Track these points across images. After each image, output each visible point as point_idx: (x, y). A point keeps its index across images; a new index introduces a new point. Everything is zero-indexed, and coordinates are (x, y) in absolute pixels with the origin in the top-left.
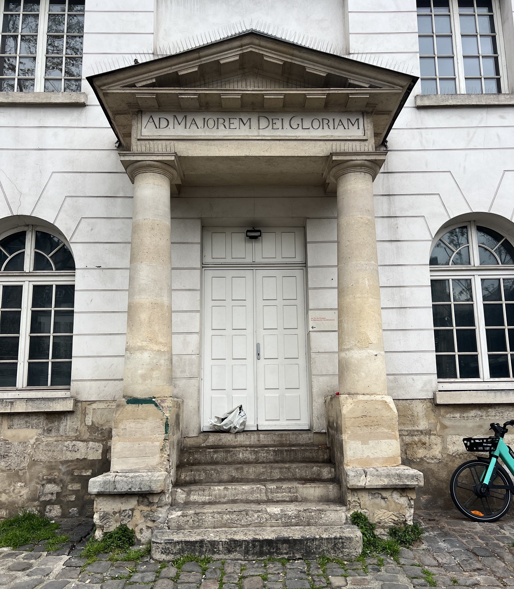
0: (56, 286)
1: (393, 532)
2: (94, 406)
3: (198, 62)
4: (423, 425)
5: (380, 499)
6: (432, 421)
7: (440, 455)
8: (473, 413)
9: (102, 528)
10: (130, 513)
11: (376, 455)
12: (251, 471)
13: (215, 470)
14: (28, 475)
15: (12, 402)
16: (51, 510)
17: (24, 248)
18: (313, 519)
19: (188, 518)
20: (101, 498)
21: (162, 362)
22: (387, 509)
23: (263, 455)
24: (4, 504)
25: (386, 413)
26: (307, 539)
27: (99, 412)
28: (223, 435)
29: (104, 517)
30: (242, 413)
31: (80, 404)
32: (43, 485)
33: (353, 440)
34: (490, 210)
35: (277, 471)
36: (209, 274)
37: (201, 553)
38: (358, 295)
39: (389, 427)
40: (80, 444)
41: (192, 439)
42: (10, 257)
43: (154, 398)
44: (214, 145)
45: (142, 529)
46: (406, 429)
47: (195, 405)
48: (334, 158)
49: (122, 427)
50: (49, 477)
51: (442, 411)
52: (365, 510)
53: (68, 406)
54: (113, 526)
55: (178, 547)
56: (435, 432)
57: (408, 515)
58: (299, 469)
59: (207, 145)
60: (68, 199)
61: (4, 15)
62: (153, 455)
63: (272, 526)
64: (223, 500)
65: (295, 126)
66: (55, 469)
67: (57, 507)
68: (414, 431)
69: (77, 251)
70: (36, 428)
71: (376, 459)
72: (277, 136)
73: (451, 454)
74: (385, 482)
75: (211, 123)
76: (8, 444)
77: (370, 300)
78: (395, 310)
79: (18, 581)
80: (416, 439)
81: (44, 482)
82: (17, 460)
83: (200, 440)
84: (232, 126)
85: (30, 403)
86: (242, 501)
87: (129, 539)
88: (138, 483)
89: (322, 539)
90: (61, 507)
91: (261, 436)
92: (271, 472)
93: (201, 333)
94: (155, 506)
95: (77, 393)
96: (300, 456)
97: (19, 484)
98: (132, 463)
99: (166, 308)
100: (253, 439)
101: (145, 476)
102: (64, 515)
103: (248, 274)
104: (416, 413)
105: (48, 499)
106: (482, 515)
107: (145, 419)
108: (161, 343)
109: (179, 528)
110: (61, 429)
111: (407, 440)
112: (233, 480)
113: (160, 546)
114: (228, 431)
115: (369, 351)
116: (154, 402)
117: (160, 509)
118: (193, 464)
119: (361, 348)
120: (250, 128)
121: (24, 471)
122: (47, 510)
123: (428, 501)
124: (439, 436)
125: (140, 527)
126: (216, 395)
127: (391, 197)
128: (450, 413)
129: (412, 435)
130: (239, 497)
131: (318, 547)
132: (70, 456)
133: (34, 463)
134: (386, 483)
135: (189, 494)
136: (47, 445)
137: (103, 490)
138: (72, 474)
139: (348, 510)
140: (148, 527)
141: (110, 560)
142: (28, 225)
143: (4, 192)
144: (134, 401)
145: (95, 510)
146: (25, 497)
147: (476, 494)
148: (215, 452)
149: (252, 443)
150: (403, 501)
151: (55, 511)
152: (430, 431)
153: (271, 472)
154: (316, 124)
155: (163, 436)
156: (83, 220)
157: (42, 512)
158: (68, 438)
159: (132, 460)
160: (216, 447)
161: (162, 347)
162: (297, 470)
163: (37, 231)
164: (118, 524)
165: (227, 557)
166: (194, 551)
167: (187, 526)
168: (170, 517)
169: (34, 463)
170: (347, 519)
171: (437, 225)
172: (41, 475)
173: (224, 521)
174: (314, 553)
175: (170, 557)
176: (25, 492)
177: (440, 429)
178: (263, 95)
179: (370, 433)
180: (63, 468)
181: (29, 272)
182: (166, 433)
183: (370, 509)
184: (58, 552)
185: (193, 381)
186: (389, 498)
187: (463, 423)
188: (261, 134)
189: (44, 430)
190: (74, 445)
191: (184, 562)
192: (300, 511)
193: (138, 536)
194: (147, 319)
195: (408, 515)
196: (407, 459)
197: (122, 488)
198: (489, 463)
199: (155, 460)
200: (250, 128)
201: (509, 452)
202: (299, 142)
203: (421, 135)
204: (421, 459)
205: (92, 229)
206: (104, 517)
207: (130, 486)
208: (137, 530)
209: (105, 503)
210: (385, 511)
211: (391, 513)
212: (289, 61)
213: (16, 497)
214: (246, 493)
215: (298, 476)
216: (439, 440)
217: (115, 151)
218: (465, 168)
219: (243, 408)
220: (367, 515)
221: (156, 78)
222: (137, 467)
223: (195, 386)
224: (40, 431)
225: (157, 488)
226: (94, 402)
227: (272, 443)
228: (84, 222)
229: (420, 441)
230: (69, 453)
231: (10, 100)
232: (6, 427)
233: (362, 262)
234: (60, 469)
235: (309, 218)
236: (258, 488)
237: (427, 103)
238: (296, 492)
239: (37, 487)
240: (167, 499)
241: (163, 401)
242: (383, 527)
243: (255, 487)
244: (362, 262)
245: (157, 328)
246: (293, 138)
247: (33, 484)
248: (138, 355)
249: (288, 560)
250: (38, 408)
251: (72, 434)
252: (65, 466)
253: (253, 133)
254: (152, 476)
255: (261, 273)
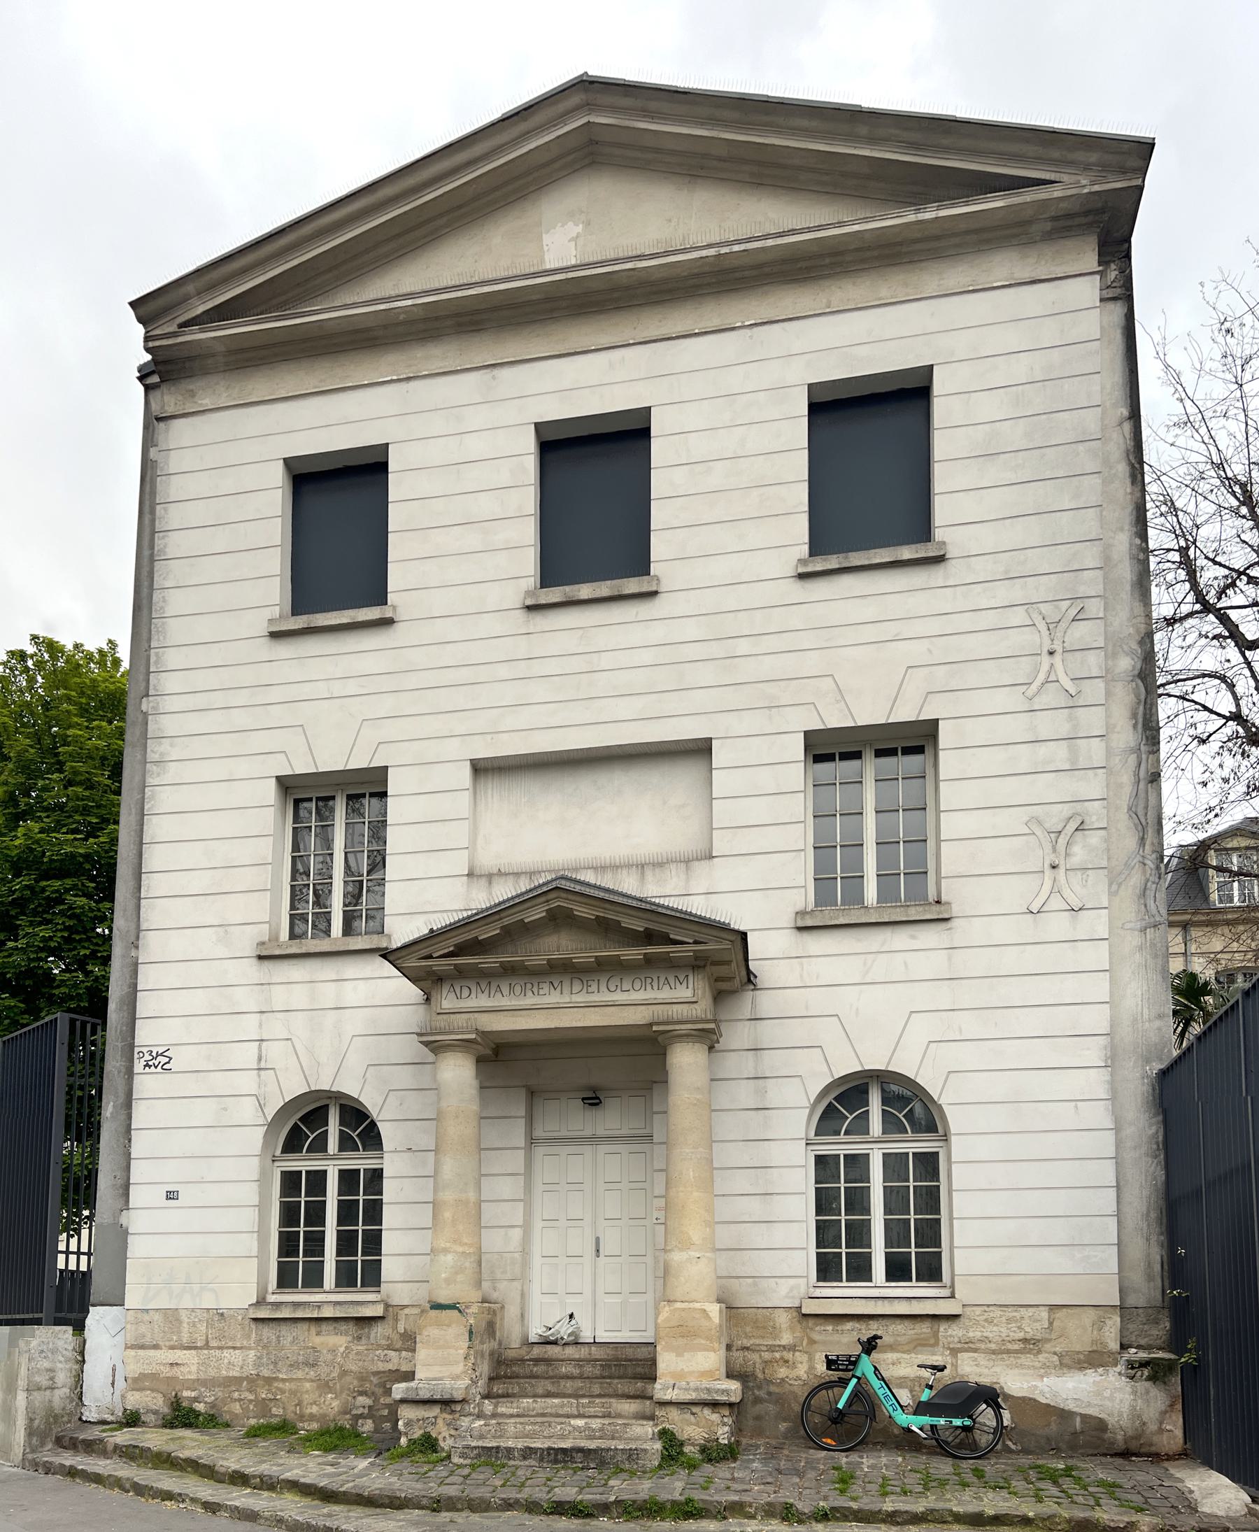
0: (364, 1170)
1: (703, 1450)
2: (407, 1311)
3: (499, 924)
4: (786, 1339)
5: (689, 1414)
6: (798, 1334)
7: (805, 1375)
8: (849, 1325)
9: (406, 1434)
10: (434, 1420)
11: (691, 1369)
12: (569, 1386)
13: (529, 1383)
14: (338, 1386)
15: (319, 1305)
16: (363, 1425)
17: (327, 1125)
18: (618, 1433)
19: (490, 1428)
20: (405, 1405)
21: (467, 1264)
22: (697, 1425)
23: (588, 1369)
24: (316, 1416)
25: (705, 1323)
26: (602, 1449)
27: (411, 1318)
28: (549, 1347)
29: (409, 1424)
30: (573, 1322)
31: (391, 1309)
32: (354, 1397)
33: (667, 1351)
34: (887, 1067)
35: (597, 1386)
36: (540, 1151)
37: (497, 1458)
38: (681, 1189)
39: (707, 1338)
40: (392, 1353)
41: (514, 1351)
42: (312, 1137)
43: (459, 1303)
44: (521, 1016)
45: (445, 1437)
46: (766, 1343)
47: (518, 1312)
48: (655, 1028)
49: (426, 1333)
50: (360, 1389)
51: (811, 1322)
52: (673, 1426)
53: (378, 1311)
54: (417, 1434)
55: (475, 1452)
56: (801, 1348)
57: (720, 1432)
58: (622, 1386)
59: (513, 1016)
60: (370, 1068)
61: (293, 828)
62: (457, 1363)
63: (574, 1439)
64: (531, 1413)
65: (613, 989)
66: (366, 1380)
67: (369, 1422)
68: (775, 1345)
69: (384, 1129)
70: (345, 1335)
71: (691, 1373)
72: (591, 1002)
73: (819, 1374)
74: (692, 1396)
75: (518, 989)
76: (317, 1352)
77: (695, 1194)
78: (758, 1197)
79: (326, 1471)
80: (777, 1355)
81: (355, 1394)
82: (327, 1370)
83: (523, 1352)
84: (590, 990)
85: (338, 1307)
86: (551, 1415)
87: (433, 1446)
88: (439, 1390)
89: (616, 1449)
90: (374, 1421)
91: (593, 1348)
92: (590, 1387)
93: (527, 1227)
94: (457, 1415)
95: (388, 1296)
96: (630, 1371)
97: (330, 1396)
98: (434, 1372)
99: (471, 1204)
100: (583, 1352)
101: (448, 1383)
102: (376, 1431)
103: (587, 1150)
104: (778, 1325)
105: (359, 1413)
106: (834, 1443)
107: (449, 1326)
108: (466, 1244)
109: (482, 1437)
110: (372, 1335)
111: (766, 1356)
112: (549, 1395)
113: (458, 1450)
114: (555, 1343)
115: (690, 1253)
116: (457, 1308)
117: (462, 1418)
118: (510, 1378)
119: (681, 1250)
120: (562, 993)
121: (334, 1381)
122: (359, 1424)
123: (788, 1430)
124: (806, 1353)
125: (443, 1434)
126: (547, 1299)
127: (758, 1052)
128: (821, 1325)
129: (773, 1351)
130: (549, 1410)
131: (613, 1457)
132: (381, 1367)
133: (344, 1373)
134: (694, 1397)
135: (496, 1406)
136: (356, 1354)
137: (405, 1396)
138: (385, 1387)
139: (656, 1425)
140: (451, 1436)
141: (412, 1461)
142: (330, 1098)
143: (300, 1064)
144: (437, 1306)
145: (399, 1417)
146: (336, 1409)
147: (830, 1419)
148: (534, 1365)
149: (582, 1357)
150: (715, 1417)
151: (367, 1426)
152: (795, 1346)
153: (590, 1387)
154: (637, 985)
155: (467, 1345)
156: (391, 1093)
157: (354, 1426)
158: (379, 1347)
159: (437, 1368)
160: (537, 1361)
161: (467, 1248)
162: (619, 1386)
163: (341, 1105)
164: (421, 1432)
165: (522, 1463)
166: (490, 1456)
167: (489, 1436)
168: (473, 1426)
169: (344, 1373)
170: (653, 1434)
171: (816, 1088)
172: (351, 1387)
173: (526, 1432)
174: (609, 1463)
175: (468, 1461)
176: (335, 1404)
177: (807, 1345)
178: (571, 958)
179: (686, 1344)
180: (375, 1380)
181: (334, 1155)
182: (470, 1340)
183: (679, 1424)
184: (365, 1456)
185: (517, 1284)
186: (700, 1414)
187: (836, 1337)
188: (573, 1000)
189: (354, 1337)
190: (386, 1355)
191: (480, 1465)
192: (604, 1424)
193: (442, 1444)
194: (451, 1218)
195: (720, 1432)
196: (765, 1379)
197: (425, 1395)
198: (848, 1384)
199: (459, 1368)
200: (562, 993)
201: (875, 1373)
202: (616, 1007)
203: (802, 964)
204: (783, 1379)
205: (401, 1104)
206: (409, 1424)
207: (432, 1393)
208: (440, 1438)
209: (408, 1410)
210: (695, 1427)
211: (701, 1430)
212: (602, 915)
213: (327, 1410)
214: (556, 1406)
215: (620, 1392)
216: (805, 1358)
217: (423, 1006)
218: (857, 1009)
219: (575, 1315)
220: (675, 1431)
221: (455, 945)
222: (440, 1375)
223: (517, 1289)
224: (349, 1338)
225: (458, 1395)
226: (406, 1306)
227: (606, 1357)
228: (392, 1097)
229: (782, 1358)
230: (380, 1363)
231: (303, 950)
232: (314, 1333)
233: (687, 1151)
234: (371, 1381)
235: (655, 1082)
236: (569, 1402)
237: (809, 923)
238: (610, 1408)
239: (348, 1400)
240: (471, 1408)
241: (467, 1307)
242: (693, 1444)
243: (565, 1400)
244: (687, 1151)
245: (461, 1228)
246: (610, 1003)
247: (344, 1396)
248: (442, 1258)
249: (582, 1469)
250: (347, 1313)
251: (384, 1342)
252: (376, 1378)
253: (565, 999)
254: (455, 1384)
255: (603, 1148)
